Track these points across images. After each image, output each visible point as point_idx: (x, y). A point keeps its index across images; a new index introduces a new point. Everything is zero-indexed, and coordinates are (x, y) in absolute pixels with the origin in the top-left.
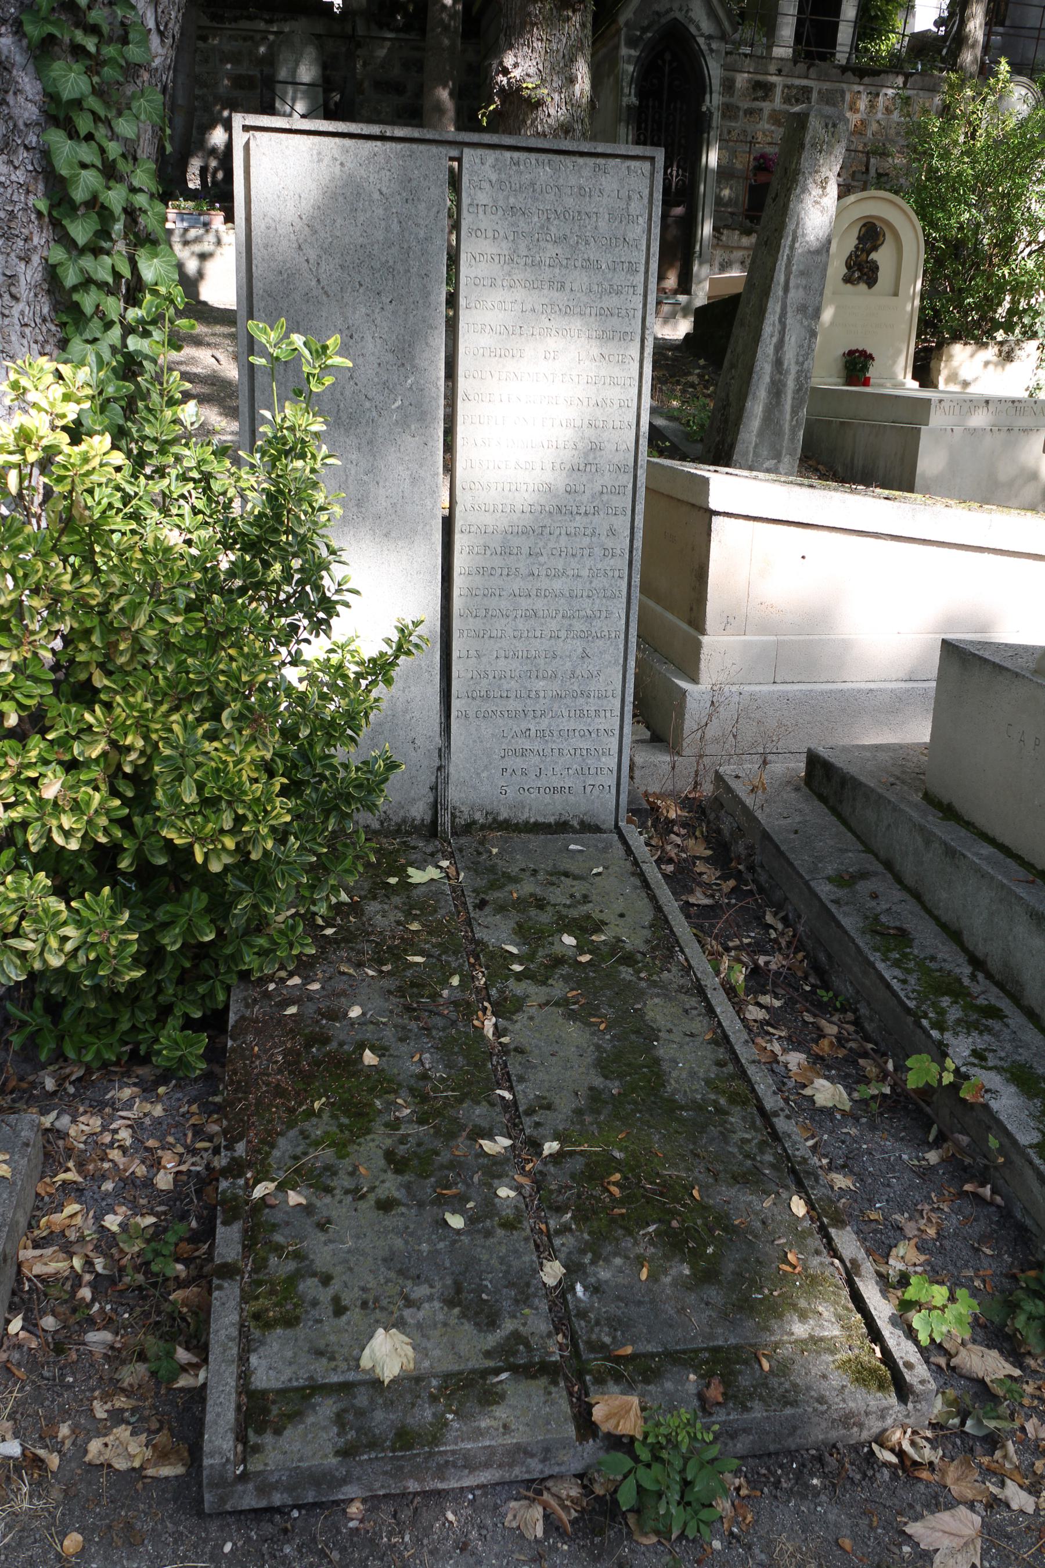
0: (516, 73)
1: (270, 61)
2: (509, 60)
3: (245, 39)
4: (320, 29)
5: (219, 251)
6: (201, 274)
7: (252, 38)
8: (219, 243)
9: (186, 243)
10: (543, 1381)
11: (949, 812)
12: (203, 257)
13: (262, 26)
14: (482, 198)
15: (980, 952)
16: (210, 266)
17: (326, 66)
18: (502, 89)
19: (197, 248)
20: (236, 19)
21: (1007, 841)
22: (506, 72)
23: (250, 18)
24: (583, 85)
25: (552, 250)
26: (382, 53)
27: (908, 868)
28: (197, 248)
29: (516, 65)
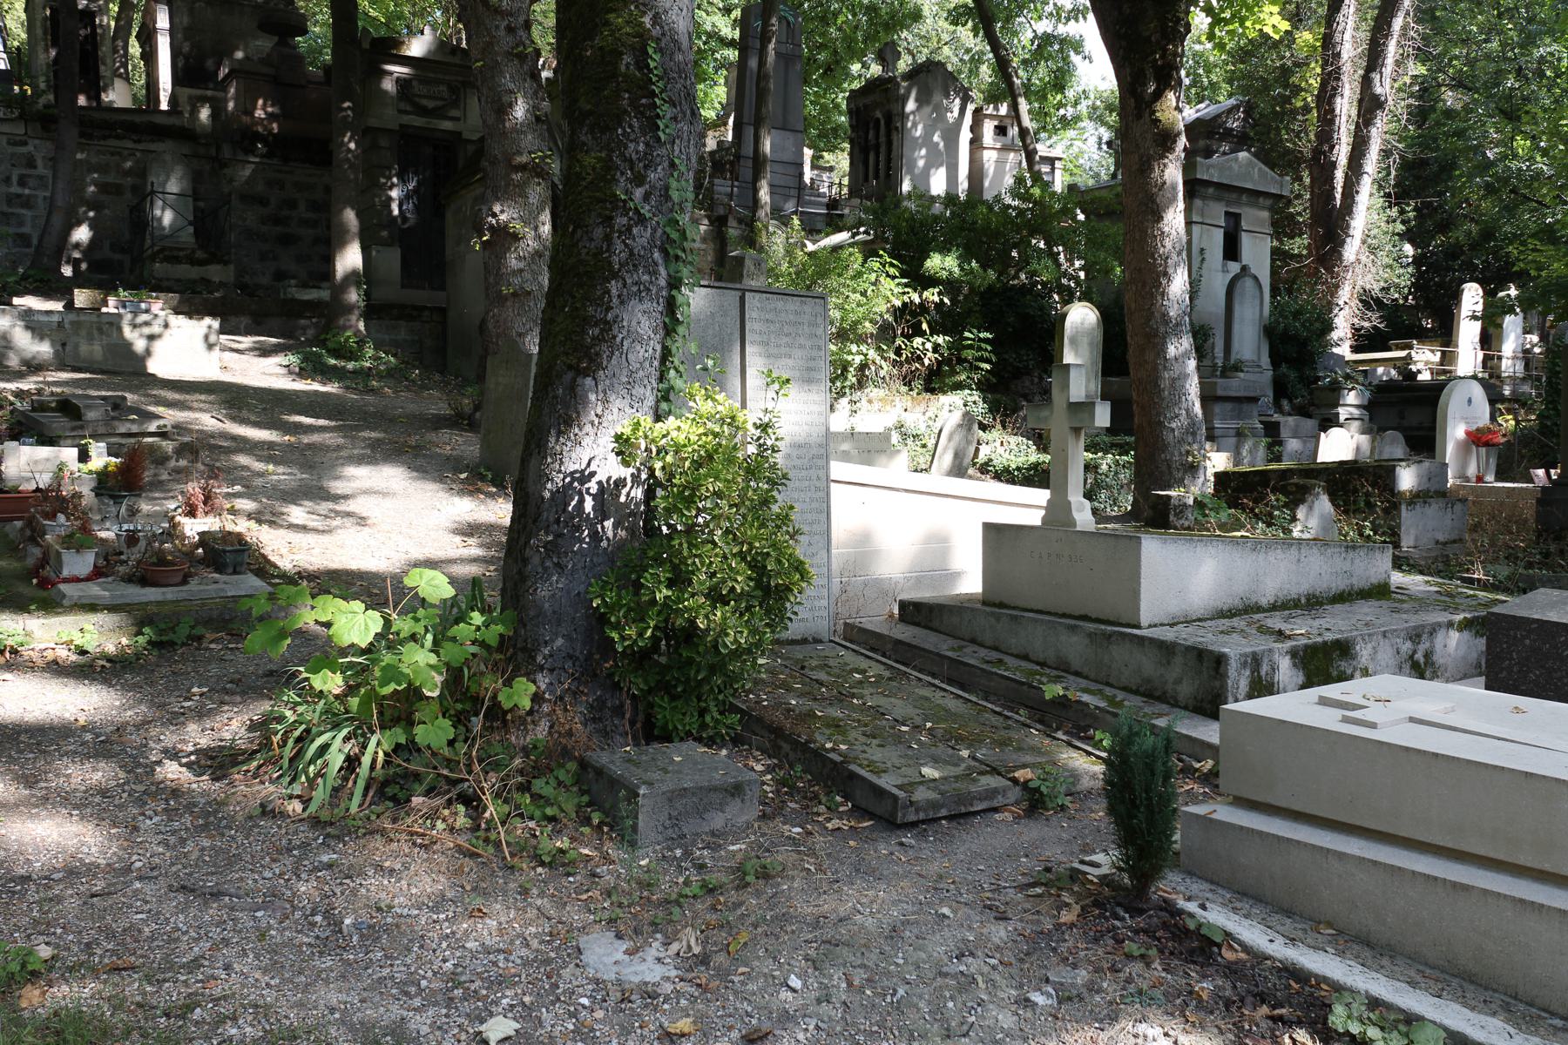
0: (503, 217)
1: (141, 172)
2: (497, 208)
3: (112, 154)
4: (186, 151)
5: (168, 332)
6: (148, 352)
7: (119, 154)
8: (166, 326)
9: (135, 326)
10: (1483, 450)
11: (1002, 605)
12: (151, 338)
13: (130, 145)
14: (754, 315)
15: (1041, 659)
16: (158, 346)
17: (196, 178)
18: (491, 226)
19: (146, 331)
20: (105, 138)
21: (1040, 607)
22: (494, 215)
23: (118, 137)
24: (546, 229)
25: (785, 340)
26: (247, 172)
27: (988, 638)
28: (146, 331)
29: (502, 212)
